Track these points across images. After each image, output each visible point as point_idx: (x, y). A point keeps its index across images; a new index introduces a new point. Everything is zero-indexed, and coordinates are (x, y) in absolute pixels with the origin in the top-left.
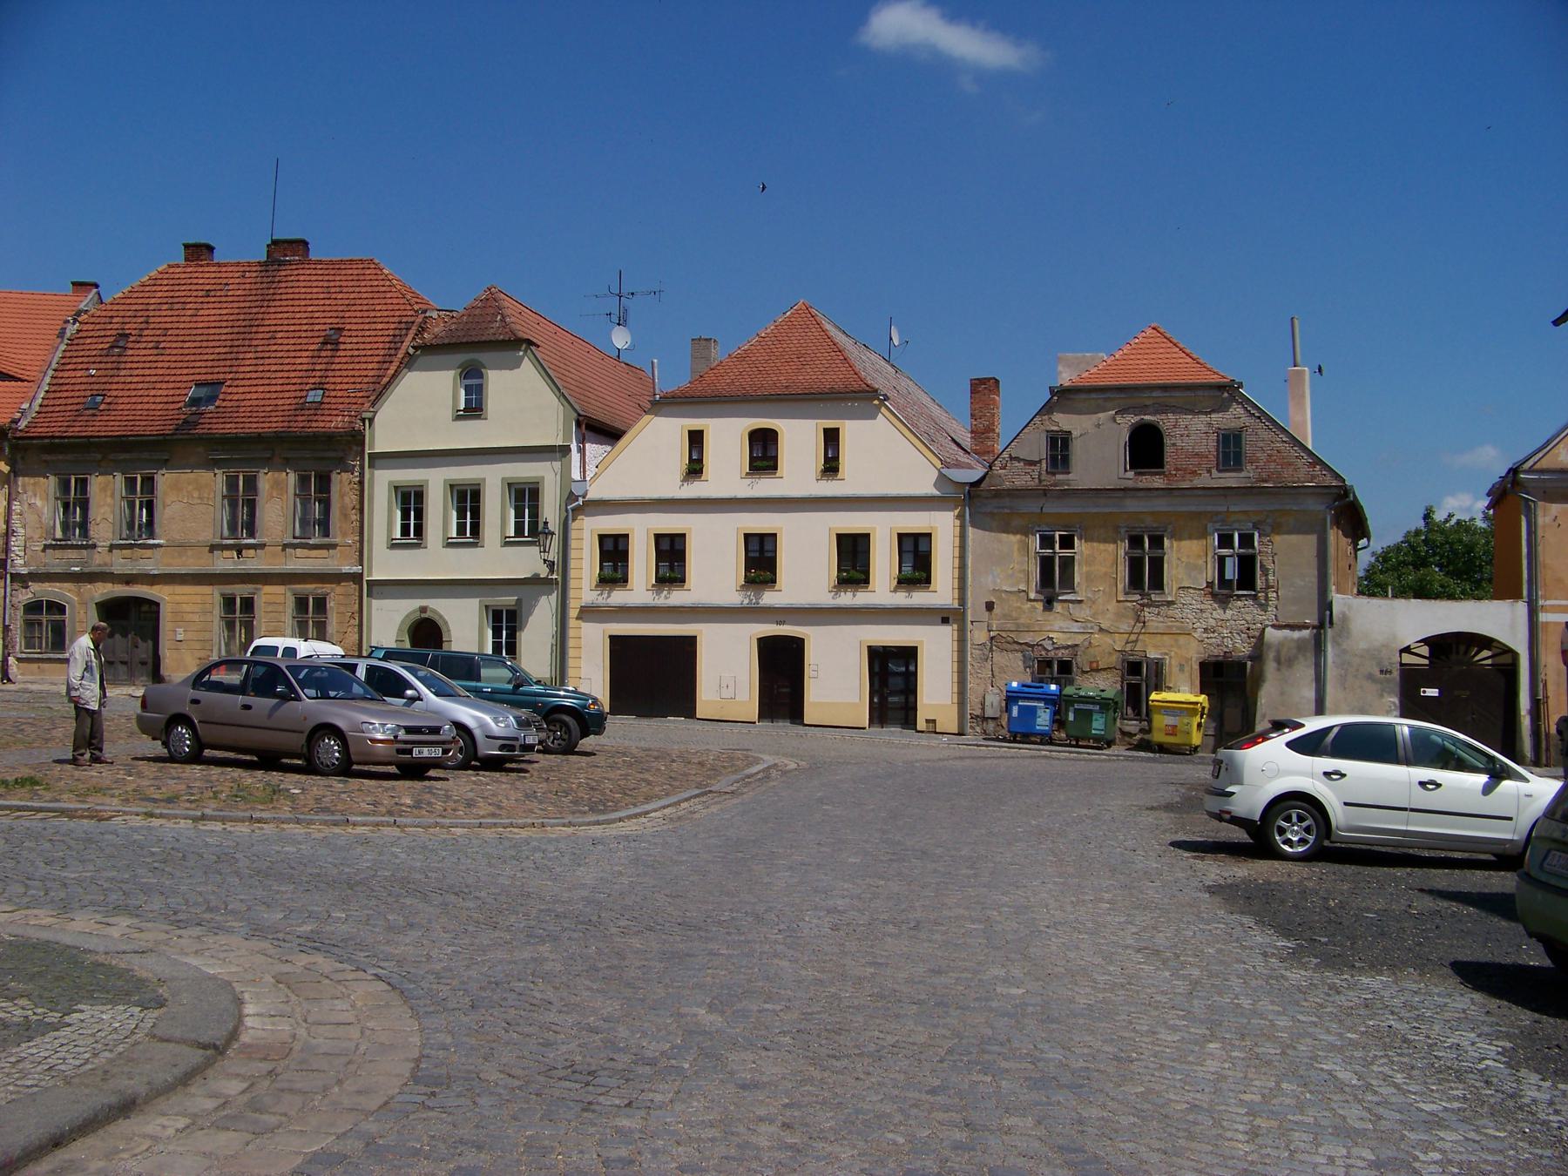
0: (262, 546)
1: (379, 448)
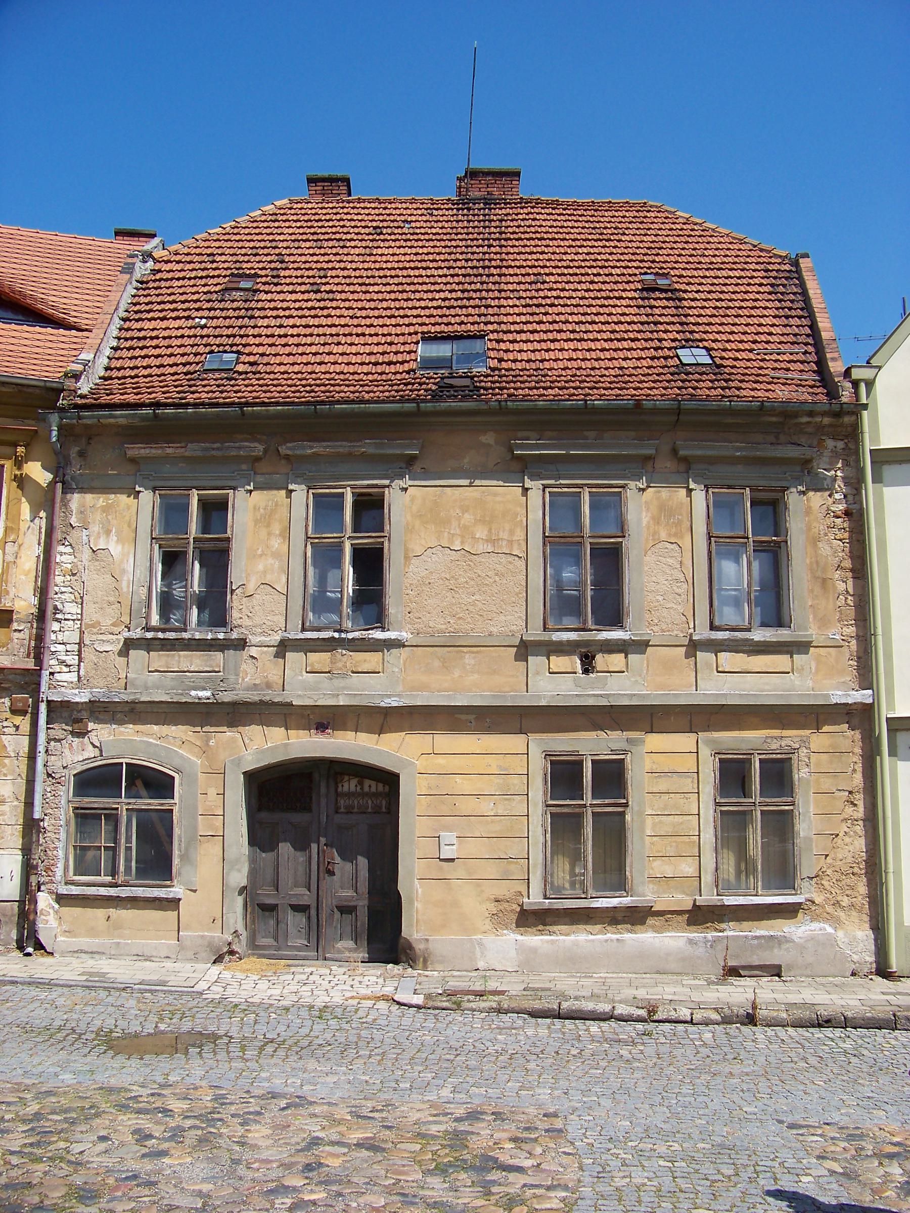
0: (641, 646)
1: (887, 443)
